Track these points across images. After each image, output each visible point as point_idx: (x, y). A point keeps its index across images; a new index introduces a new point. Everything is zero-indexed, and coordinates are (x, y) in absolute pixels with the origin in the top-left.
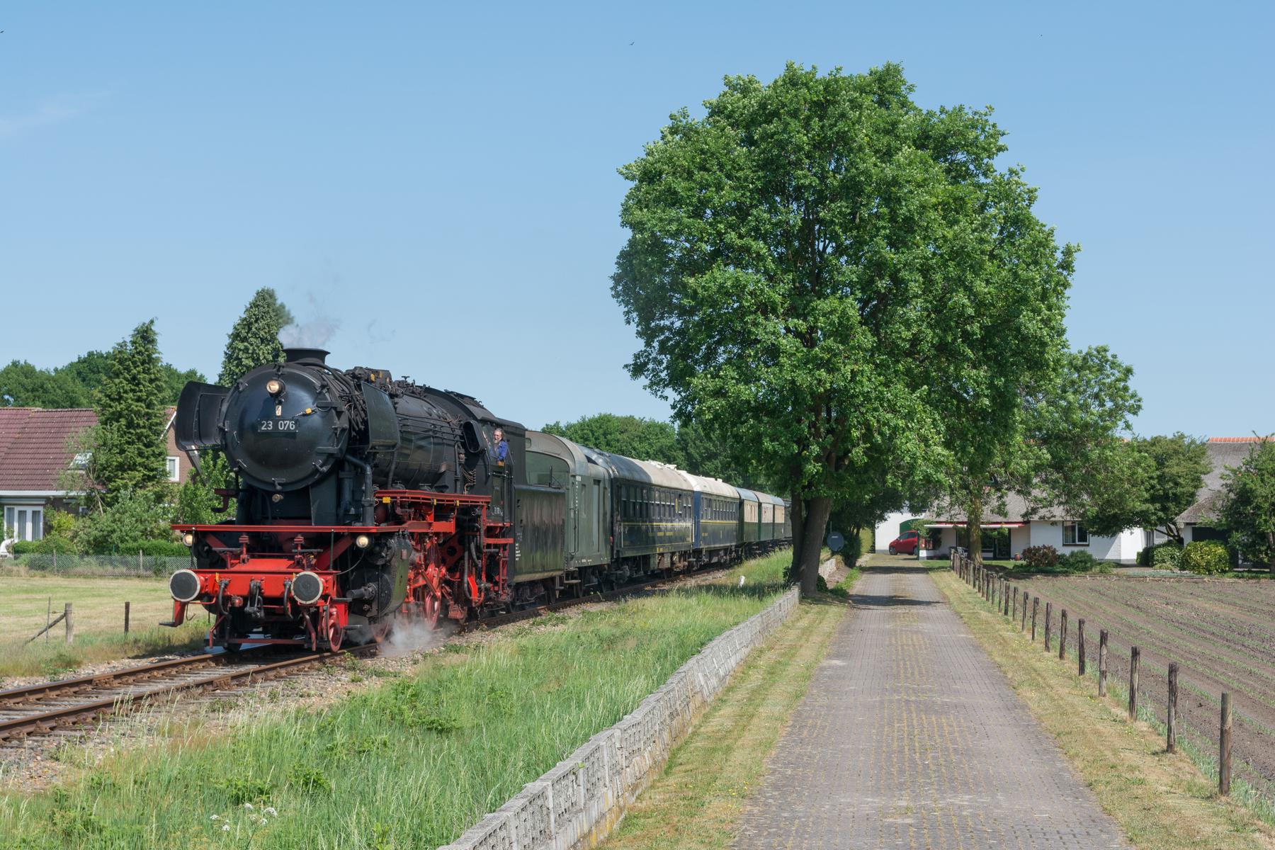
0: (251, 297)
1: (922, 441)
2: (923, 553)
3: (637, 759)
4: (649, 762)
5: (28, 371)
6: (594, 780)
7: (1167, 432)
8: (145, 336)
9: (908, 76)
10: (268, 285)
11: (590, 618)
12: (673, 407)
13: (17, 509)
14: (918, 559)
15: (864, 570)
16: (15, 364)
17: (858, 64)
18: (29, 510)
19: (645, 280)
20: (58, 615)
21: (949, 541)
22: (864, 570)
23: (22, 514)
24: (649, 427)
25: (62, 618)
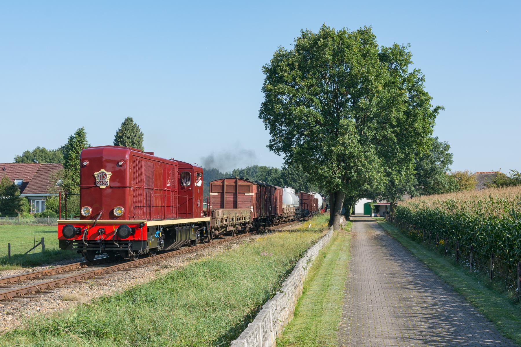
0: (123, 121)
1: (376, 172)
2: (373, 215)
3: (283, 312)
4: (288, 313)
5: (43, 151)
6: (266, 330)
7: (462, 170)
8: (80, 134)
9: (374, 31)
10: (130, 116)
11: (252, 240)
12: (284, 159)
13: (36, 201)
14: (371, 216)
15: (352, 221)
16: (38, 148)
17: (352, 28)
18: (40, 201)
19: (270, 112)
20: (39, 242)
21: (382, 210)
22: (352, 221)
23: (38, 202)
24: (271, 170)
25: (40, 243)
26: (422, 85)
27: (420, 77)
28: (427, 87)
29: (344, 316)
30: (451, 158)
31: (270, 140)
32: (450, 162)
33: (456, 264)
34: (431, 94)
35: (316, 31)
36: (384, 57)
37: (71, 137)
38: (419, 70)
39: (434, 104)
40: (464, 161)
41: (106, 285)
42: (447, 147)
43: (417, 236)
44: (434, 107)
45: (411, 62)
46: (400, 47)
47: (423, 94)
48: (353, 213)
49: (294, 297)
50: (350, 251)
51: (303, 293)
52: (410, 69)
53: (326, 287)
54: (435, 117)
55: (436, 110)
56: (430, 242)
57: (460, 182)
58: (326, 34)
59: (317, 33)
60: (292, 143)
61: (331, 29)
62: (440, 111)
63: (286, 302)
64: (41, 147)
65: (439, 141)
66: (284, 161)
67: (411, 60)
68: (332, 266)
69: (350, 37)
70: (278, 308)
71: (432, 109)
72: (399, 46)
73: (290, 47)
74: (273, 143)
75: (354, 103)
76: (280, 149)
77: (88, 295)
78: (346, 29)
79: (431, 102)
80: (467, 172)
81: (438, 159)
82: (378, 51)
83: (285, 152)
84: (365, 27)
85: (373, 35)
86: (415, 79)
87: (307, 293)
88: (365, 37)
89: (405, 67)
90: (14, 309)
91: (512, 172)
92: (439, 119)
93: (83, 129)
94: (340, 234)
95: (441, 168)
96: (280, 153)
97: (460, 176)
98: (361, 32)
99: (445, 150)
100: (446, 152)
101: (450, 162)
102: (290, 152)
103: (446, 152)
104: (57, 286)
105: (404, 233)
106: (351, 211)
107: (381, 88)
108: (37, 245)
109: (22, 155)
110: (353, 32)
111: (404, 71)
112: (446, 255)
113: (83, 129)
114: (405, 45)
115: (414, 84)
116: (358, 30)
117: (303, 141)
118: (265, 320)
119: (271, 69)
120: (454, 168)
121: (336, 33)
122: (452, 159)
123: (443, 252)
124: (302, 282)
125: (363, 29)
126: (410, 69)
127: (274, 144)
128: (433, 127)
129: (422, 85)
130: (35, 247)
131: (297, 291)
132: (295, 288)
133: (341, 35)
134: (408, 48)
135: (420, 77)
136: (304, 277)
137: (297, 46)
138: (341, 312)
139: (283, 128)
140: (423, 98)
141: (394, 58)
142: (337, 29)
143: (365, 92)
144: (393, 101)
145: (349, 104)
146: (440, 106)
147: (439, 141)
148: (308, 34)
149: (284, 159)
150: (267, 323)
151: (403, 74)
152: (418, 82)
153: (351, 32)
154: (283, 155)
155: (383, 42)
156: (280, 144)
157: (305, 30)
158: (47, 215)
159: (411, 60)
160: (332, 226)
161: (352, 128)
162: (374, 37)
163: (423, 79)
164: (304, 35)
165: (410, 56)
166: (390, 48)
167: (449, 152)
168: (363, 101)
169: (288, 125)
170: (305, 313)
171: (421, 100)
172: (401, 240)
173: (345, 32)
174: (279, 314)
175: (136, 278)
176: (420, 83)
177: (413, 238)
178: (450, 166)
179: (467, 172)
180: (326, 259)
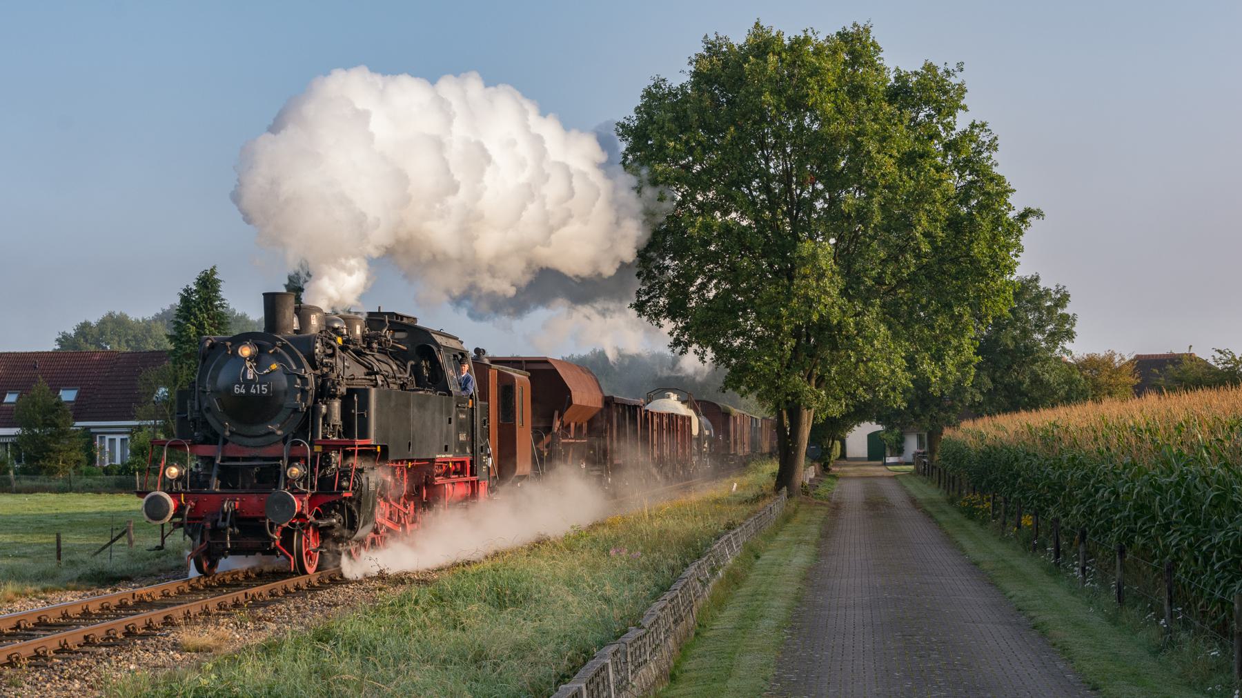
4: (655, 672)
7: (1100, 351)
9: (876, 35)
13: (108, 437)
17: (824, 31)
18: (118, 438)
26: (989, 158)
27: (987, 140)
28: (1002, 164)
29: (777, 681)
30: (1073, 325)
31: (638, 292)
32: (1070, 335)
33: (1055, 571)
34: (1011, 180)
35: (739, 38)
36: (901, 94)
37: (186, 291)
38: (983, 125)
39: (1017, 202)
40: (1101, 332)
41: (270, 620)
42: (1063, 299)
43: (978, 510)
44: (1019, 209)
45: (964, 108)
46: (939, 72)
47: (992, 180)
48: (843, 455)
49: (671, 641)
50: (818, 545)
51: (697, 634)
52: (961, 122)
53: (747, 622)
54: (1020, 232)
55: (1023, 217)
56: (1004, 523)
57: (1092, 380)
58: (762, 45)
59: (742, 42)
60: (687, 296)
61: (774, 34)
62: (1032, 219)
63: (649, 650)
64: (117, 313)
65: (1042, 285)
66: (672, 339)
67: (962, 103)
68: (770, 579)
69: (818, 52)
70: (629, 659)
71: (1011, 215)
72: (935, 68)
73: (679, 77)
74: (644, 298)
75: (832, 202)
76: (662, 311)
77: (233, 641)
78: (810, 34)
79: (1011, 199)
80: (1111, 357)
81: (1040, 327)
82: (886, 80)
83: (673, 319)
84: (855, 25)
85: (874, 44)
86: (974, 145)
87: (708, 634)
88: (855, 46)
89: (950, 119)
90: (82, 668)
91: (1218, 355)
92: (1030, 237)
93: (213, 271)
94: (803, 506)
95: (1049, 349)
96: (662, 321)
97: (1091, 364)
98: (843, 36)
99: (1056, 305)
100: (1060, 311)
101: (1070, 335)
102: (684, 317)
103: (1060, 311)
104: (168, 622)
105: (952, 501)
106: (837, 451)
107: (892, 169)
108: (118, 538)
109: (73, 333)
110: (828, 39)
111: (949, 127)
112: (1035, 550)
113: (213, 271)
114: (952, 66)
115: (970, 155)
116: (838, 33)
117: (714, 291)
118: (598, 679)
119: (637, 128)
120: (1077, 349)
121: (787, 42)
122: (1074, 329)
123: (1032, 544)
124: (694, 609)
125: (850, 30)
126: (961, 122)
127: (648, 301)
128: (1017, 256)
129: (989, 158)
130: (113, 541)
131: (681, 628)
132: (675, 622)
133: (798, 45)
134: (958, 74)
135: (987, 140)
136: (701, 601)
137: (696, 74)
138: (770, 673)
139: (667, 262)
140: (990, 188)
141: (930, 93)
142: (790, 33)
143: (855, 176)
144: (919, 197)
145: (819, 204)
146: (1034, 208)
147: (1042, 285)
148: (721, 46)
149: (671, 334)
150: (601, 687)
151: (944, 135)
152: (980, 153)
153: (822, 38)
154: (668, 325)
155: (898, 58)
156: (663, 301)
157: (712, 38)
158: (134, 470)
159: (962, 103)
160: (785, 489)
161: (826, 262)
162: (878, 49)
163: (993, 146)
164: (713, 49)
165: (961, 90)
166: (916, 73)
167: (1068, 310)
168: (851, 198)
169: (678, 255)
170: (694, 674)
171: (987, 190)
172: (942, 518)
173: (806, 41)
174: (632, 672)
175: (336, 605)
176: (985, 155)
177: (970, 513)
178: (1068, 345)
179: (1111, 357)
180: (759, 562)
